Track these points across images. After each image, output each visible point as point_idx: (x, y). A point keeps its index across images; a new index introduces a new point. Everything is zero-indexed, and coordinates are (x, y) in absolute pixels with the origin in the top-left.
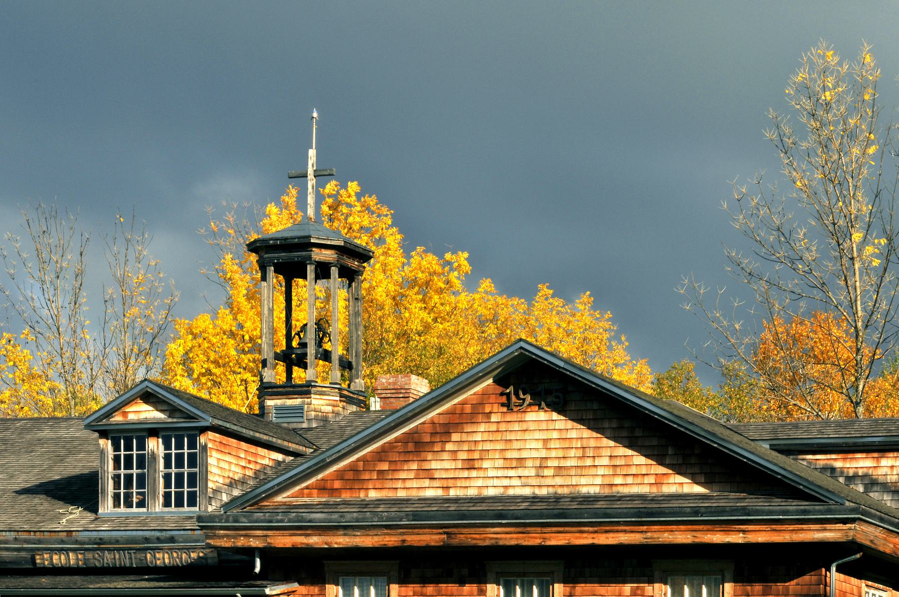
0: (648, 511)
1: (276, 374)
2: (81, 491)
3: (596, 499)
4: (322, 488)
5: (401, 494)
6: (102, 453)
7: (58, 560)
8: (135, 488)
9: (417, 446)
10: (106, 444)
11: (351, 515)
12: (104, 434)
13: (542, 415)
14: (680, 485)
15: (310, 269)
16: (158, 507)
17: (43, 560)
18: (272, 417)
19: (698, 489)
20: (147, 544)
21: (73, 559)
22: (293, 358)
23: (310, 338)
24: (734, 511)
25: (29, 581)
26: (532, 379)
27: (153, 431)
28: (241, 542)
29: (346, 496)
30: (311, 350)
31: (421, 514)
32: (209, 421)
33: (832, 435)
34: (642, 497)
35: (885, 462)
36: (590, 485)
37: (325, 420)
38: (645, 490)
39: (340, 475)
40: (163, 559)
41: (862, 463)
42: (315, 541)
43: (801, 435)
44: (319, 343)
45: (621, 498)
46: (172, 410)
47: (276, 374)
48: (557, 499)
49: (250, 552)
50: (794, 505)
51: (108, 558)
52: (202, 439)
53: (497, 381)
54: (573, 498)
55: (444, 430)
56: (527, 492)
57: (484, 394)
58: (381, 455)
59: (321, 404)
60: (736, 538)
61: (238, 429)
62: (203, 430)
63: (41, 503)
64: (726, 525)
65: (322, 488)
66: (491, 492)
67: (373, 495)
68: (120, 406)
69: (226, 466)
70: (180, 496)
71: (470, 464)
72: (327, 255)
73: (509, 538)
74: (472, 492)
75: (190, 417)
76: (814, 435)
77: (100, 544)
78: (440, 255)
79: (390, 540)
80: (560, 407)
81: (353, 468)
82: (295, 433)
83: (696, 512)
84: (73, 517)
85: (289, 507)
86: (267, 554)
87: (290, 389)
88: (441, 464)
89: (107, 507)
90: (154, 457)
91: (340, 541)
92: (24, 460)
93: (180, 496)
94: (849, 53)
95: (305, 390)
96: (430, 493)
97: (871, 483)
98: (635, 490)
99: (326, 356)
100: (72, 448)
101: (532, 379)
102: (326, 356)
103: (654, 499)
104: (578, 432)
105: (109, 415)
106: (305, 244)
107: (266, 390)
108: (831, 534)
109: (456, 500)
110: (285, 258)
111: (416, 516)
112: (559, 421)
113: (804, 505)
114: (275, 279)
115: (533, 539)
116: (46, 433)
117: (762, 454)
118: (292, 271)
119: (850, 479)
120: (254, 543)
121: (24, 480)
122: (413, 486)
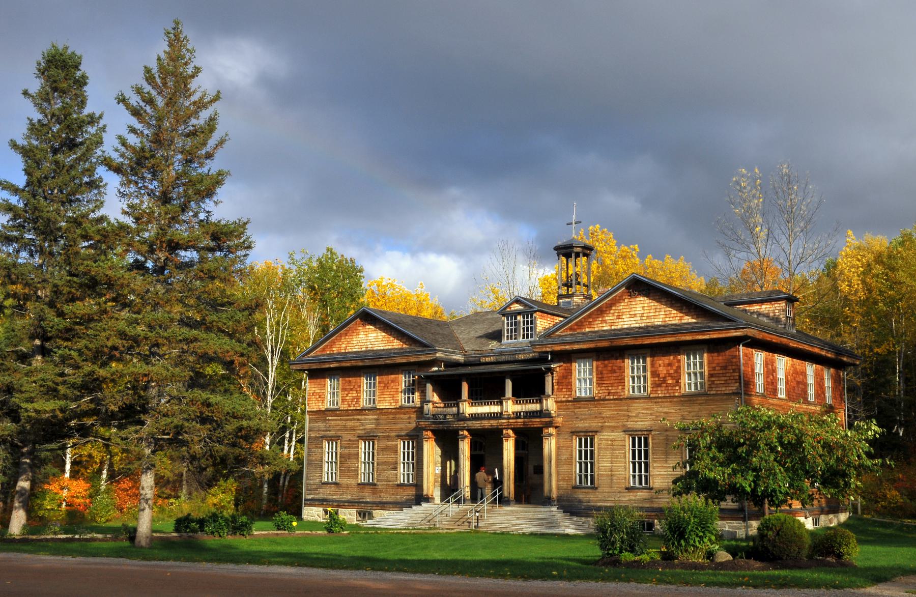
0: (677, 329)
1: (564, 291)
2: (496, 336)
3: (660, 326)
4: (571, 329)
5: (596, 329)
6: (503, 322)
7: (488, 360)
8: (514, 333)
9: (601, 312)
10: (504, 319)
11: (579, 338)
12: (504, 315)
13: (642, 299)
14: (688, 319)
15: (573, 255)
16: (521, 339)
17: (483, 360)
18: (562, 305)
19: (694, 321)
20: (516, 352)
21: (492, 359)
22: (568, 285)
23: (573, 278)
24: (705, 327)
25: (477, 368)
26: (639, 286)
27: (519, 313)
28: (544, 350)
29: (578, 331)
30: (574, 282)
31: (602, 335)
32: (536, 308)
33: (745, 299)
34: (675, 325)
35: (764, 307)
36: (658, 321)
37: (578, 305)
38: (676, 322)
39: (576, 324)
40: (522, 357)
41: (756, 307)
42: (568, 347)
43: (735, 299)
44: (577, 279)
45: (668, 325)
46: (526, 305)
47: (564, 291)
48: (647, 327)
49: (547, 352)
50: (726, 324)
51: (504, 358)
52: (535, 315)
53: (627, 288)
54: (652, 326)
55: (610, 306)
56: (637, 325)
57: (623, 292)
58: (589, 316)
59: (577, 300)
60: (707, 337)
61: (547, 310)
62: (535, 312)
63: (484, 340)
64: (703, 332)
65: (571, 329)
66: (625, 326)
67: (587, 330)
68: (509, 306)
69: (542, 323)
70: (511, 336)
71: (619, 317)
72: (579, 250)
73: (632, 342)
74: (619, 327)
75: (532, 308)
76: (739, 299)
77: (501, 353)
78: (628, 246)
79: (592, 345)
80: (647, 295)
81: (581, 321)
82: (569, 311)
83: (693, 328)
84: (493, 345)
85: (560, 336)
86: (552, 353)
87: (568, 296)
88: (609, 318)
89: (504, 341)
90: (519, 322)
91: (576, 347)
92: (481, 326)
93: (511, 336)
94: (750, 169)
95: (572, 296)
96: (606, 328)
97: (759, 314)
98: (673, 322)
99: (579, 284)
100: (497, 321)
101: (639, 286)
102: (579, 284)
103: (679, 325)
104: (653, 304)
105: (505, 309)
106: (571, 247)
107: (560, 296)
108: (738, 333)
109: (614, 330)
110: (566, 251)
111: (600, 336)
112: (647, 300)
113: (729, 323)
114: (564, 259)
115: (639, 342)
116: (490, 316)
117: (719, 308)
118: (568, 256)
119: (752, 313)
120: (548, 349)
121: (480, 333)
122: (602, 326)
